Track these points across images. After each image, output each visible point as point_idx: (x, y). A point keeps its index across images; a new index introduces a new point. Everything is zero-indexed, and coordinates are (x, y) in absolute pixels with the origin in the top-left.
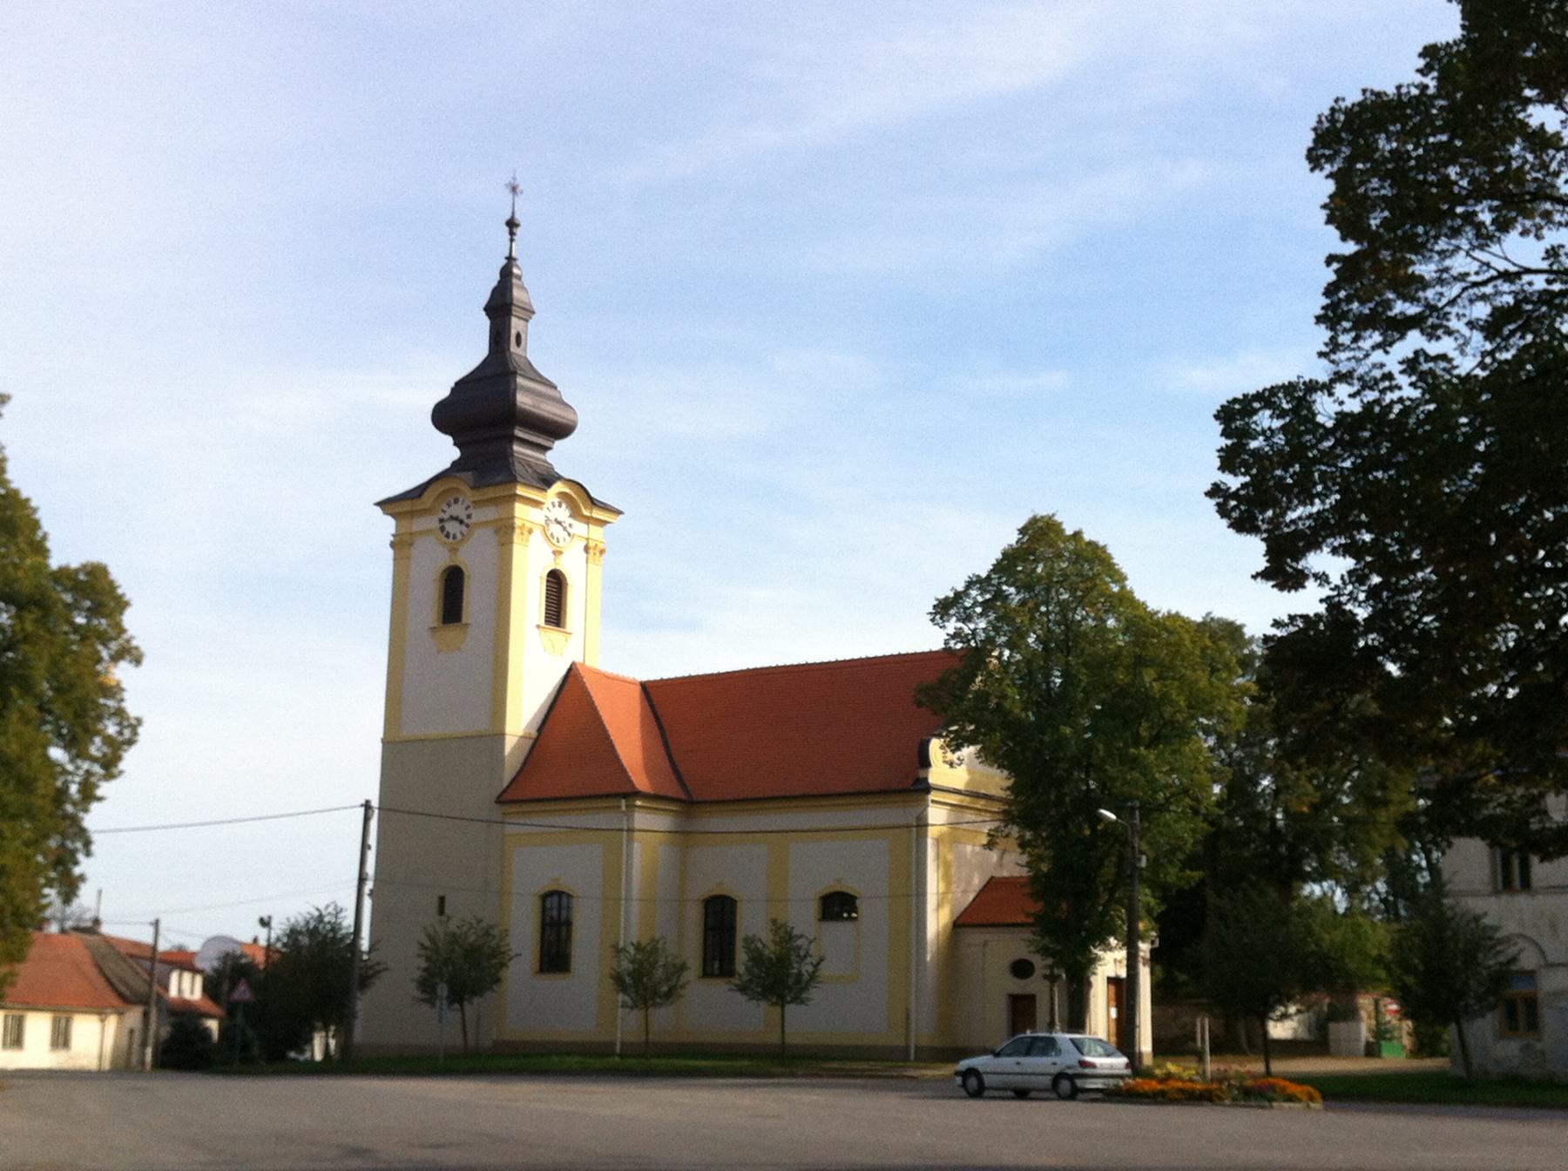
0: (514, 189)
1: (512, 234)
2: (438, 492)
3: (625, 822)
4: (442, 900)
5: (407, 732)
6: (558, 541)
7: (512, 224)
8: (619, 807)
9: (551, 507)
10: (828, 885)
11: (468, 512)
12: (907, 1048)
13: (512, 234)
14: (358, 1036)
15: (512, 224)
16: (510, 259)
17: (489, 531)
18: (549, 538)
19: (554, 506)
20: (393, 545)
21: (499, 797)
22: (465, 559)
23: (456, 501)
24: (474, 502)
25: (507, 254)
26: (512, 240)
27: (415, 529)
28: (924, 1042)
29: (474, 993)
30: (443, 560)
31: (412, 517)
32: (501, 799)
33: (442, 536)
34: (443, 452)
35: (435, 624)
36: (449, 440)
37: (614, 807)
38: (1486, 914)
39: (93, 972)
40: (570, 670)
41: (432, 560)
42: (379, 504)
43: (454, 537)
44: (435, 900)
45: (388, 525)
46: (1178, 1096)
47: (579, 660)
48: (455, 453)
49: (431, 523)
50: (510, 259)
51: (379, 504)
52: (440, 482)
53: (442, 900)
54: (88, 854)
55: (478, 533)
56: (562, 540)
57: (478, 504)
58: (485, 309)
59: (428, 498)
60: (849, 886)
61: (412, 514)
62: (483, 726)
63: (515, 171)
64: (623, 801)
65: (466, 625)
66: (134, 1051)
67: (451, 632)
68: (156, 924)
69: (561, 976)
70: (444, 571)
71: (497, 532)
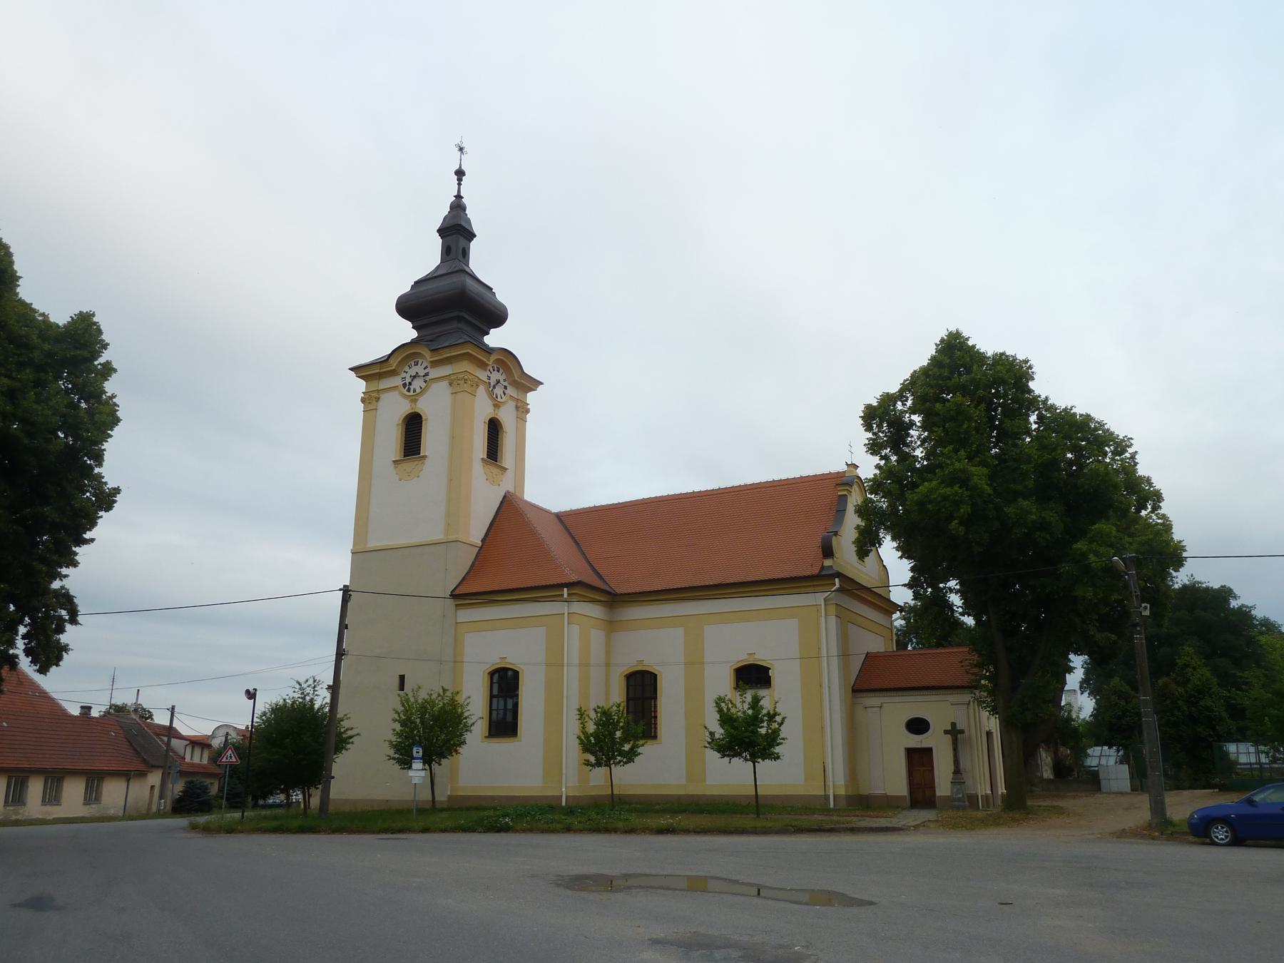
0: (461, 149)
1: (460, 180)
4: (402, 678)
5: (373, 544)
6: (497, 397)
7: (460, 173)
9: (492, 370)
10: (742, 658)
11: (426, 371)
12: (826, 797)
13: (460, 180)
14: (333, 794)
15: (460, 173)
17: (445, 383)
18: (491, 394)
19: (494, 370)
20: (363, 400)
22: (423, 406)
23: (416, 364)
24: (431, 362)
26: (459, 184)
27: (381, 388)
28: (842, 792)
29: (442, 756)
30: (405, 408)
31: (380, 379)
33: (405, 391)
34: (406, 332)
36: (410, 324)
38: (394, 730)
40: (505, 497)
41: (395, 408)
43: (414, 391)
44: (397, 680)
45: (361, 385)
46: (928, 824)
47: (512, 490)
48: (414, 334)
49: (396, 381)
53: (402, 678)
54: (73, 621)
55: (436, 387)
56: (499, 397)
57: (435, 364)
58: (438, 231)
59: (393, 364)
60: (762, 658)
61: (380, 376)
63: (357, 728)
64: (565, 589)
65: (425, 457)
67: (410, 465)
68: (385, 741)
70: (404, 419)
71: (451, 384)
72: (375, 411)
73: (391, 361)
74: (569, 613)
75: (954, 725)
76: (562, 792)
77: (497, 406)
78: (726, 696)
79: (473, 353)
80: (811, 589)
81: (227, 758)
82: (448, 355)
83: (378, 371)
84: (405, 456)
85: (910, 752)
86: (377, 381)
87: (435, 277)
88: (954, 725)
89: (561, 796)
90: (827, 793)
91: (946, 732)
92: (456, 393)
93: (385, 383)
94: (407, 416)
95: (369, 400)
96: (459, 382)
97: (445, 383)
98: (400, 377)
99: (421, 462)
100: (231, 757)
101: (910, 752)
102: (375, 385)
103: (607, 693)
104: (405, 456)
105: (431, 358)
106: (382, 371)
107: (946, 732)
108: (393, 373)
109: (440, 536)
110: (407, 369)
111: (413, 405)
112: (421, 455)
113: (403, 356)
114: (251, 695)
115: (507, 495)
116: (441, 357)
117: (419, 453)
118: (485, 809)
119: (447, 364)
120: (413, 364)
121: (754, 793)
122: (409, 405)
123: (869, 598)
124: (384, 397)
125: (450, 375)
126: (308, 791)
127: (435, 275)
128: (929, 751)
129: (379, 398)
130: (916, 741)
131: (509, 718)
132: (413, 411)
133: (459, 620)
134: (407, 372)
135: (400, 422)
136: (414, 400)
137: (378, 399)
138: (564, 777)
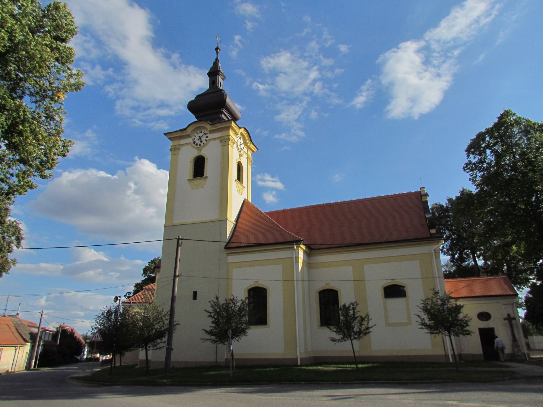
2: (193, 128)
3: (294, 254)
4: (195, 293)
8: (293, 247)
12: (447, 356)
13: (217, 52)
16: (217, 59)
21: (226, 246)
22: (204, 152)
23: (201, 132)
25: (216, 58)
30: (195, 153)
32: (228, 246)
33: (194, 145)
35: (191, 178)
37: (290, 248)
39: (14, 330)
40: (244, 201)
42: (165, 134)
44: (192, 294)
49: (190, 140)
50: (217, 59)
51: (165, 134)
52: (195, 124)
53: (195, 293)
55: (212, 143)
57: (212, 132)
59: (189, 131)
61: (181, 138)
62: (215, 216)
65: (207, 177)
66: (298, 367)
67: (199, 181)
69: (263, 326)
71: (221, 141)
73: (187, 130)
74: (296, 257)
75: (509, 315)
76: (297, 356)
77: (241, 155)
81: (95, 338)
82: (221, 127)
83: (180, 135)
84: (194, 177)
85: (481, 331)
86: (179, 140)
87: (208, 93)
88: (509, 315)
89: (297, 359)
90: (447, 353)
91: (505, 319)
92: (224, 146)
93: (182, 142)
95: (175, 150)
96: (226, 140)
97: (218, 141)
100: (98, 337)
101: (481, 331)
102: (176, 143)
103: (49, 338)
104: (194, 177)
107: (505, 319)
108: (188, 136)
110: (195, 134)
111: (199, 152)
112: (205, 176)
115: (245, 200)
116: (216, 128)
117: (203, 176)
118: (266, 367)
119: (219, 132)
120: (199, 132)
121: (145, 358)
124: (183, 148)
125: (220, 137)
127: (209, 92)
128: (492, 330)
129: (180, 149)
130: (484, 325)
133: (229, 261)
134: (195, 136)
136: (200, 150)
137: (179, 149)
138: (298, 347)
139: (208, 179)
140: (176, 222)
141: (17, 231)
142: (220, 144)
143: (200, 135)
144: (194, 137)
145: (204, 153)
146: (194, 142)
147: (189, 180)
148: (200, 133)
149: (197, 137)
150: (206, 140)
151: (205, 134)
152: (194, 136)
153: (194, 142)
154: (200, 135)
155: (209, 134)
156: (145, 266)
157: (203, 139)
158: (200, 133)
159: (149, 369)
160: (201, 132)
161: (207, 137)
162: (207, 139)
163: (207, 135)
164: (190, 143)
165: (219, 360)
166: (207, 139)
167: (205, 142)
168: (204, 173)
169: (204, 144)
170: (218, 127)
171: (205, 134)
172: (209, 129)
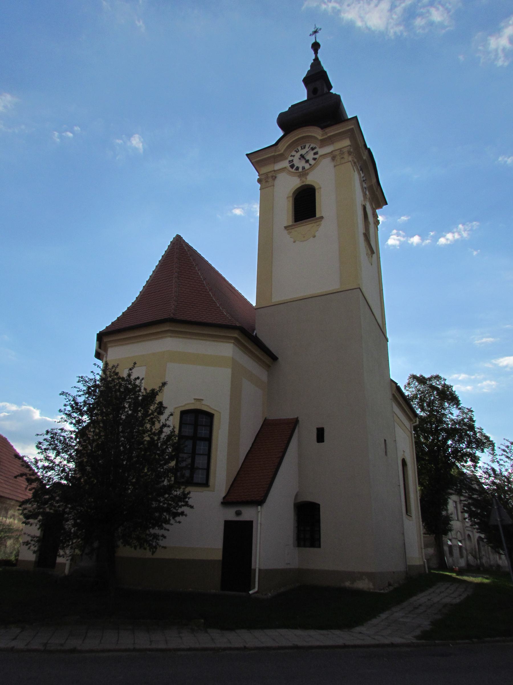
49: (285, 164)
57: (324, 143)
65: (322, 218)
67: (306, 227)
72: (272, 187)
78: (157, 401)
79: (340, 131)
80: (189, 337)
83: (273, 154)
94: (314, 187)
98: (287, 161)
99: (317, 224)
102: (265, 170)
105: (322, 136)
106: (276, 154)
108: (281, 157)
109: (334, 285)
110: (294, 153)
112: (318, 215)
113: (294, 139)
114: (170, 421)
117: (315, 216)
122: (299, 180)
123: (243, 341)
126: (452, 570)
129: (276, 177)
131: (418, 463)
132: (304, 184)
134: (294, 156)
135: (291, 195)
136: (304, 173)
137: (274, 178)
139: (323, 222)
140: (276, 299)
141: (419, 491)
142: (332, 164)
143: (303, 152)
144: (290, 159)
145: (311, 179)
146: (292, 166)
147: (286, 228)
148: (302, 149)
149: (298, 155)
150: (314, 159)
151: (313, 149)
152: (292, 156)
153: (292, 166)
154: (303, 152)
155: (320, 148)
156: (99, 332)
157: (310, 156)
158: (302, 149)
159: (175, 467)
160: (304, 148)
161: (316, 153)
162: (316, 156)
163: (315, 151)
164: (285, 168)
165: (410, 563)
166: (316, 156)
167: (312, 162)
168: (315, 213)
169: (310, 165)
170: (329, 135)
171: (313, 149)
172: (320, 138)
